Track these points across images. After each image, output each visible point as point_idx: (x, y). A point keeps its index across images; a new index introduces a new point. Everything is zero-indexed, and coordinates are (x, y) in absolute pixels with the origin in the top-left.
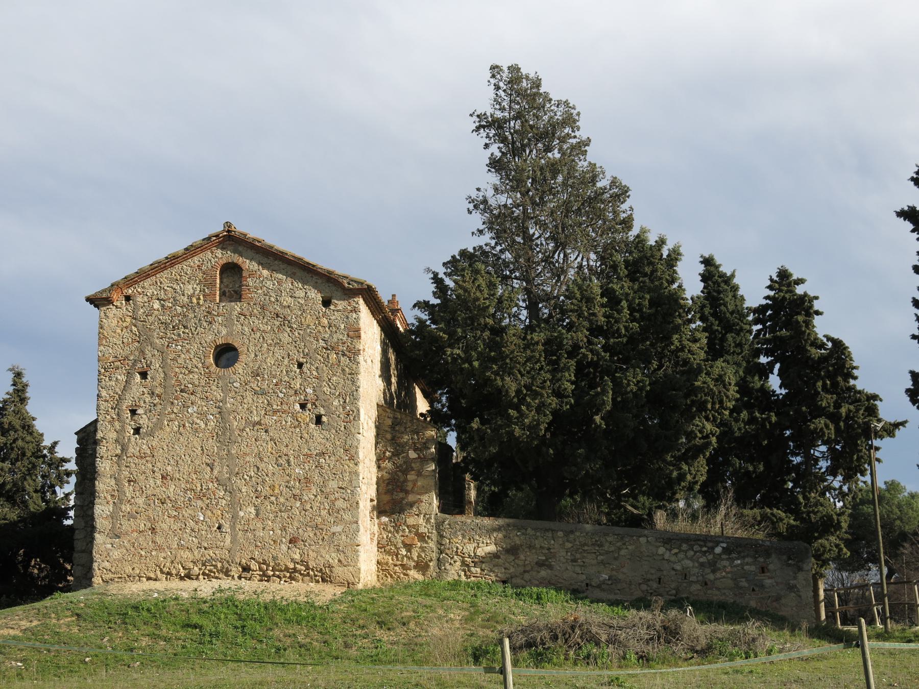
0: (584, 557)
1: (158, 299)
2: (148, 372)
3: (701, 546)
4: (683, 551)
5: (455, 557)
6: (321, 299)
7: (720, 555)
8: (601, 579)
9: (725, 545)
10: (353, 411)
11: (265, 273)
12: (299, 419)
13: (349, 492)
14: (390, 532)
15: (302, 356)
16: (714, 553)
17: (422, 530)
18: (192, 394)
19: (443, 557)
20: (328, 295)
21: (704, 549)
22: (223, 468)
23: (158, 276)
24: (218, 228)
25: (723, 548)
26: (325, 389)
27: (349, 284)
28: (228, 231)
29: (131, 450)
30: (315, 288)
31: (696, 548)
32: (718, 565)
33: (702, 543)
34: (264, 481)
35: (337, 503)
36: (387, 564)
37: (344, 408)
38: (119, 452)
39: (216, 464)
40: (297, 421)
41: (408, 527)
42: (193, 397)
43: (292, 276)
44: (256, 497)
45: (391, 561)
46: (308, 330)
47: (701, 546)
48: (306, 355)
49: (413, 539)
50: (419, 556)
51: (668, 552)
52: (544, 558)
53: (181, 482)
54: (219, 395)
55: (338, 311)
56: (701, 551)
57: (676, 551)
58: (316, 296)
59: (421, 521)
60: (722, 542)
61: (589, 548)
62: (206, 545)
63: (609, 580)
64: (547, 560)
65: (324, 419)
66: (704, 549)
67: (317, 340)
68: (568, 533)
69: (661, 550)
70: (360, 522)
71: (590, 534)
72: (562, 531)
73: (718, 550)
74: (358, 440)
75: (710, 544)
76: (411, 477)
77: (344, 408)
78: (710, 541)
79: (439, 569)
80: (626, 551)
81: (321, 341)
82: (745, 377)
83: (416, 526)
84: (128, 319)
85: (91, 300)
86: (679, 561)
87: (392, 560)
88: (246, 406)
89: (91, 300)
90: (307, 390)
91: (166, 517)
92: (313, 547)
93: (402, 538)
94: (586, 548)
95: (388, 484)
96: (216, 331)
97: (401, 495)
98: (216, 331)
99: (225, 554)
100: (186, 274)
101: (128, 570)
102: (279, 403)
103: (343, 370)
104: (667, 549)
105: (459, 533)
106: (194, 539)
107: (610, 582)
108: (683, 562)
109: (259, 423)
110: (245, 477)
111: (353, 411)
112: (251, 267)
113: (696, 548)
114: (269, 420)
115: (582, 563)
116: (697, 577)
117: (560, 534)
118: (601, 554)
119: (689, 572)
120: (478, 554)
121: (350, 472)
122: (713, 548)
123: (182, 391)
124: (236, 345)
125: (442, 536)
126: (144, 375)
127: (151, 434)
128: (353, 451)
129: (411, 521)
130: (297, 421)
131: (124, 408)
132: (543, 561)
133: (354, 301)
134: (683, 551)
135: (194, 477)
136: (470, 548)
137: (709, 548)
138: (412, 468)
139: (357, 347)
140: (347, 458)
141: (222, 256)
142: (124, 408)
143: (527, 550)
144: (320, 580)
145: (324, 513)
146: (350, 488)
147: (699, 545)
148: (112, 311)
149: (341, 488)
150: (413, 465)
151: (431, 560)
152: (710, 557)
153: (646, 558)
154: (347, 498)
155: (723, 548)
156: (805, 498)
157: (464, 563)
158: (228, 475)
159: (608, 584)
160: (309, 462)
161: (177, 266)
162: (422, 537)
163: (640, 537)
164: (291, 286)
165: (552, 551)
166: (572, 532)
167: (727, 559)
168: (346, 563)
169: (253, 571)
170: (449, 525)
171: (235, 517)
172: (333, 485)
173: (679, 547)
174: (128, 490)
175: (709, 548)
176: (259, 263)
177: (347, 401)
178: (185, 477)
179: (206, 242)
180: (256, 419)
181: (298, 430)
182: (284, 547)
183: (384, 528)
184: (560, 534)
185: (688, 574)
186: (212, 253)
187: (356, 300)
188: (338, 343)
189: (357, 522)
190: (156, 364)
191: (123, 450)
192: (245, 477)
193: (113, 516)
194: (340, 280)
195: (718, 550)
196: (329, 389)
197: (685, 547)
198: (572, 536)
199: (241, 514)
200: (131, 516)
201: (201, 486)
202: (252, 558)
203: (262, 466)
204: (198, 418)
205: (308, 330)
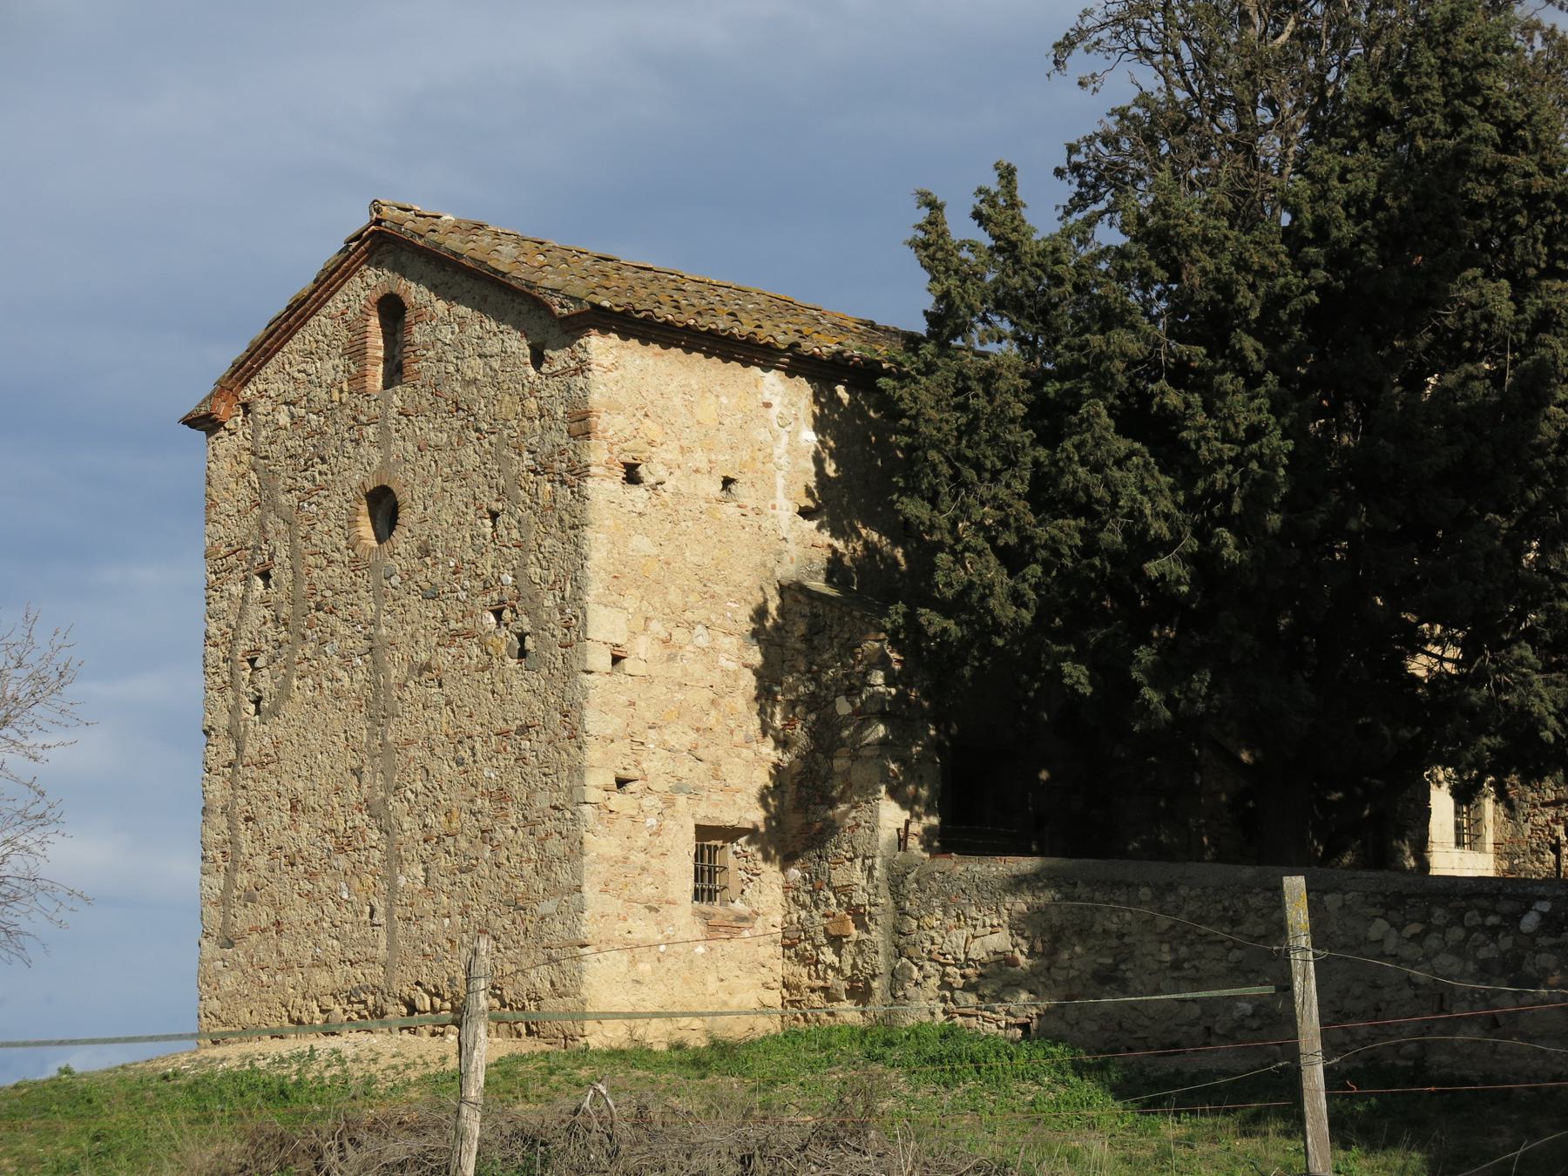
0: (1200, 956)
1: (286, 403)
2: (271, 572)
5: (927, 965)
6: (528, 351)
7: (1532, 936)
8: (1236, 1014)
9: (1545, 907)
10: (577, 617)
11: (441, 306)
12: (490, 649)
13: (568, 815)
14: (804, 906)
15: (495, 496)
17: (860, 898)
18: (331, 613)
19: (903, 966)
20: (538, 340)
21: (1492, 920)
22: (375, 777)
23: (285, 349)
24: (360, 220)
25: (1543, 915)
26: (532, 570)
27: (562, 306)
28: (378, 222)
29: (249, 750)
30: (517, 327)
31: (1472, 918)
32: (1528, 969)
33: (1485, 904)
34: (436, 805)
35: (549, 844)
36: (798, 987)
37: (562, 611)
38: (232, 755)
39: (365, 769)
40: (488, 654)
41: (834, 890)
42: (332, 618)
43: (480, 306)
44: (425, 841)
45: (805, 980)
46: (505, 432)
47: (1484, 913)
48: (502, 494)
49: (843, 921)
50: (854, 966)
51: (1394, 931)
52: (1109, 961)
53: (317, 815)
54: (368, 609)
55: (554, 375)
57: (1415, 928)
58: (518, 345)
59: (858, 876)
60: (1542, 898)
62: (352, 957)
63: (1253, 1016)
64: (1116, 966)
66: (1492, 920)
67: (520, 455)
68: (1164, 889)
69: (1379, 928)
70: (585, 888)
71: (1210, 891)
72: (1148, 885)
73: (1530, 922)
74: (585, 690)
75: (1507, 907)
76: (840, 764)
77: (562, 611)
78: (1508, 897)
79: (893, 995)
81: (526, 454)
83: (845, 890)
84: (245, 457)
85: (192, 422)
87: (809, 976)
88: (409, 628)
89: (192, 422)
90: (502, 577)
91: (296, 896)
92: (510, 953)
93: (825, 921)
94: (1204, 929)
95: (800, 784)
96: (365, 461)
98: (365, 461)
99: (376, 975)
100: (325, 336)
101: (244, 1015)
102: (460, 614)
103: (561, 520)
104: (1393, 925)
105: (936, 902)
106: (335, 942)
107: (1255, 1024)
109: (427, 667)
110: (409, 794)
111: (577, 617)
112: (419, 297)
113: (1472, 918)
114: (444, 659)
115: (1192, 973)
117: (1145, 893)
120: (972, 955)
121: (570, 768)
122: (1516, 918)
123: (318, 608)
125: (903, 912)
126: (265, 576)
128: (575, 715)
129: (839, 877)
130: (488, 654)
131: (239, 657)
133: (580, 345)
135: (335, 800)
136: (958, 937)
137: (1504, 917)
139: (584, 458)
140: (566, 734)
141: (372, 282)
142: (239, 657)
143: (1075, 940)
144: (524, 1031)
145: (528, 869)
146: (569, 806)
147: (1480, 909)
148: (225, 443)
149: (555, 808)
151: (874, 976)
152: (1506, 943)
154: (565, 833)
155: (1543, 915)
157: (945, 985)
158: (383, 794)
159: (1251, 1030)
160: (505, 749)
161: (311, 322)
162: (859, 917)
163: (1325, 892)
164: (479, 332)
165: (1127, 940)
166: (1171, 887)
167: (1552, 949)
168: (562, 989)
169: (420, 1012)
170: (917, 881)
171: (393, 888)
172: (542, 801)
173: (1426, 919)
174: (245, 836)
175: (1504, 917)
176: (433, 288)
177: (567, 594)
178: (322, 802)
180: (424, 657)
181: (487, 675)
183: (793, 899)
184: (1145, 893)
186: (362, 277)
187: (582, 341)
188: (551, 455)
189: (579, 889)
190: (283, 553)
191: (238, 751)
192: (409, 794)
194: (548, 299)
195: (1530, 922)
196: (538, 570)
197: (1439, 915)
198: (1170, 898)
199: (402, 881)
201: (346, 821)
202: (418, 983)
203: (433, 765)
204: (340, 665)
205: (505, 432)
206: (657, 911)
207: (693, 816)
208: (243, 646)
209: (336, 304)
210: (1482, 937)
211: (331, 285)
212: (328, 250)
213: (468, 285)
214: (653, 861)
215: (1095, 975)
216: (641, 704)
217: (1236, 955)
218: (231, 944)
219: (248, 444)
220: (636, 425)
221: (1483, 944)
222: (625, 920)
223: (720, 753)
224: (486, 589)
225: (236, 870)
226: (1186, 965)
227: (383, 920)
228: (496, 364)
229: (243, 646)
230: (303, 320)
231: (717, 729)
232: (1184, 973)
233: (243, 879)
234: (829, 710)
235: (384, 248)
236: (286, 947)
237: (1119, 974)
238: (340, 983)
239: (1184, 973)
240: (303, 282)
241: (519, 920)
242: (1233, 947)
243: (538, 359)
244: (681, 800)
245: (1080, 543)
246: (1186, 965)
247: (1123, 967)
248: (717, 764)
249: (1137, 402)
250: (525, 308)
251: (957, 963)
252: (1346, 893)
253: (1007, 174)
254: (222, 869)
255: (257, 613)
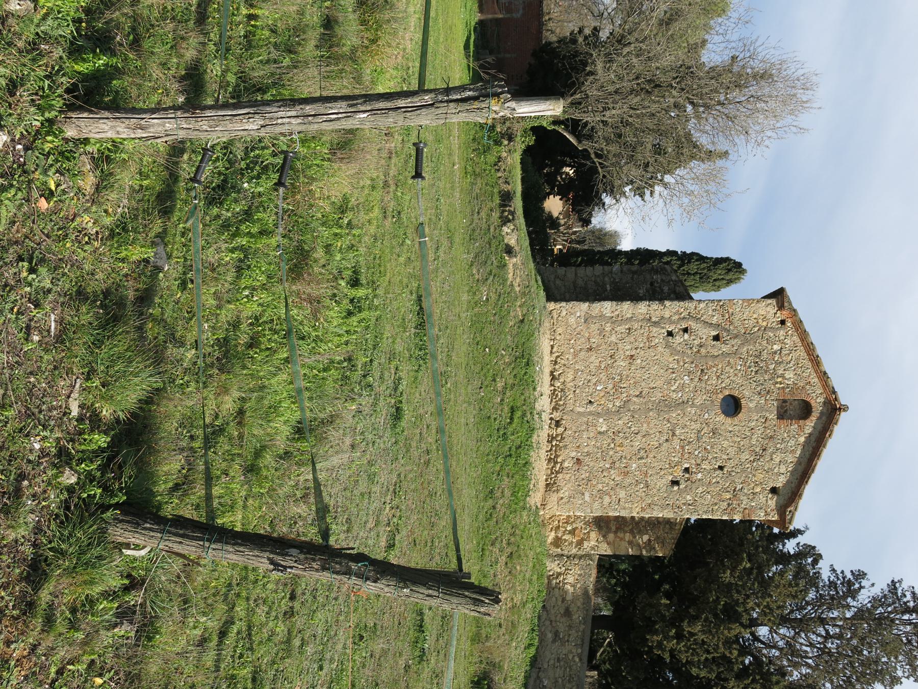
11: (802, 440)
17: (586, 544)
20: (781, 492)
24: (843, 399)
38: (654, 319)
41: (588, 532)
43: (799, 463)
48: (730, 473)
50: (566, 540)
54: (698, 401)
59: (593, 543)
62: (577, 392)
77: (684, 504)
81: (741, 486)
92: (573, 477)
94: (568, 670)
105: (582, 572)
117: (579, 651)
126: (716, 338)
141: (817, 402)
149: (619, 501)
170: (589, 564)
176: (810, 434)
180: (677, 433)
190: (725, 348)
191: (655, 323)
192: (630, 423)
194: (793, 504)
203: (639, 437)
208: (692, 324)
212: (836, 382)
213: (807, 456)
217: (560, 680)
219: (769, 325)
225: (612, 323)
227: (588, 410)
228: (776, 471)
229: (692, 324)
236: (583, 353)
238: (568, 385)
240: (827, 366)
243: (774, 490)
245: (692, 521)
250: (793, 485)
251: (564, 579)
253: (807, 528)
254: (613, 315)
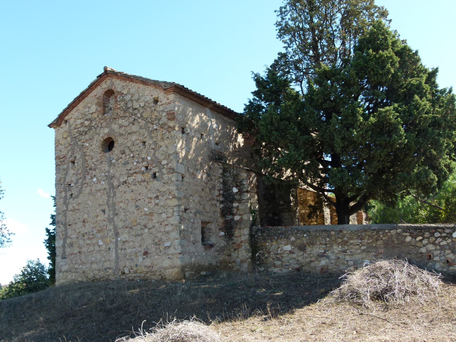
3: (440, 233)
4: (427, 238)
16: (452, 237)
21: (444, 235)
38: (65, 208)
51: (414, 239)
52: (323, 251)
56: (441, 237)
61: (355, 241)
64: (325, 252)
65: (157, 174)
72: (334, 231)
80: (382, 241)
82: (437, 96)
86: (424, 246)
97: (230, 217)
108: (427, 246)
115: (350, 253)
116: (440, 257)
118: (363, 245)
119: (433, 254)
124: (112, 137)
127: (77, 197)
132: (323, 253)
134: (427, 238)
137: (447, 234)
138: (235, 198)
147: (439, 232)
150: (236, 197)
153: (397, 246)
156: (440, 204)
163: (391, 230)
179: (99, 78)
182: (140, 259)
185: (432, 255)
193: (64, 246)
197: (427, 234)
200: (71, 245)
206: (195, 244)
207: (200, 219)
209: (94, 92)
210: (441, 240)
211: (92, 89)
214: (193, 231)
215: (318, 255)
216: (188, 189)
218: (65, 258)
220: (183, 118)
221: (442, 241)
222: (188, 247)
223: (205, 203)
224: (143, 161)
226: (348, 251)
230: (83, 98)
231: (204, 196)
232: (347, 253)
233: (68, 241)
234: (231, 191)
235: (107, 78)
237: (326, 254)
239: (347, 253)
241: (158, 248)
242: (362, 246)
244: (198, 215)
246: (348, 251)
247: (327, 252)
248: (204, 205)
249: (383, 88)
252: (397, 230)
255: (71, 172)
